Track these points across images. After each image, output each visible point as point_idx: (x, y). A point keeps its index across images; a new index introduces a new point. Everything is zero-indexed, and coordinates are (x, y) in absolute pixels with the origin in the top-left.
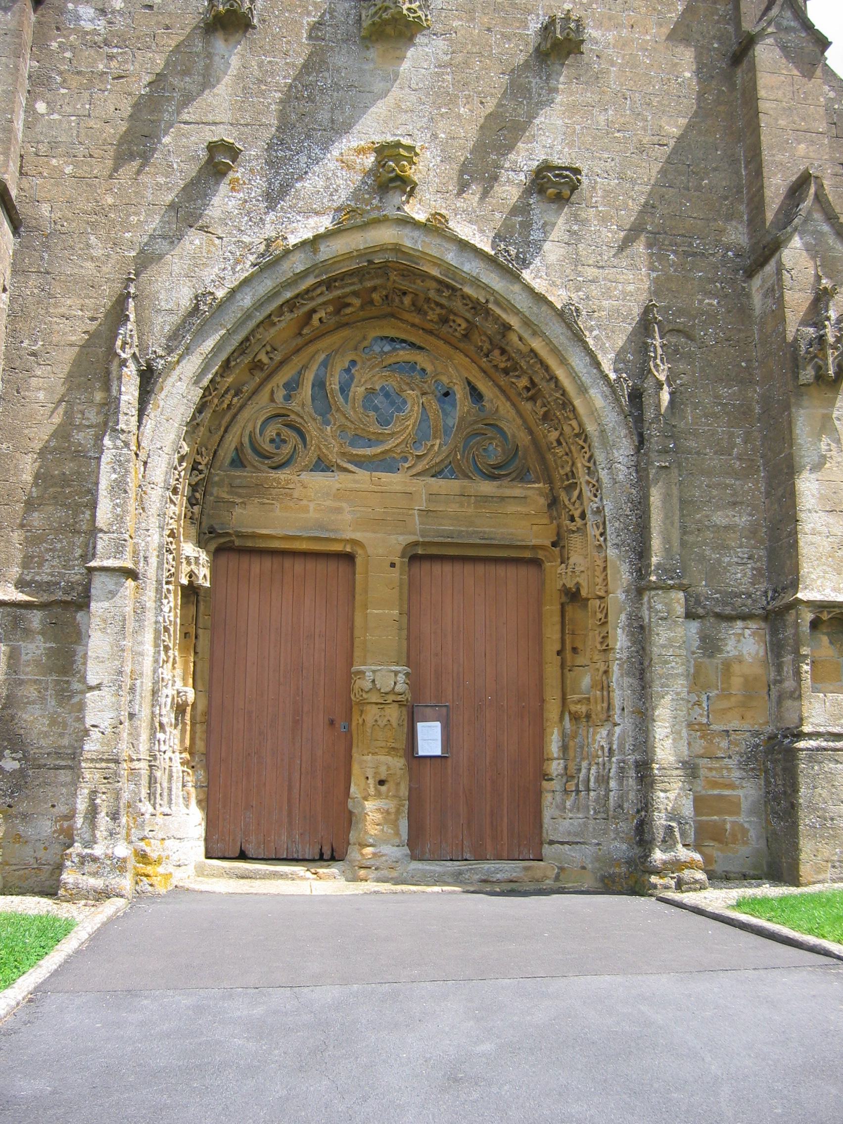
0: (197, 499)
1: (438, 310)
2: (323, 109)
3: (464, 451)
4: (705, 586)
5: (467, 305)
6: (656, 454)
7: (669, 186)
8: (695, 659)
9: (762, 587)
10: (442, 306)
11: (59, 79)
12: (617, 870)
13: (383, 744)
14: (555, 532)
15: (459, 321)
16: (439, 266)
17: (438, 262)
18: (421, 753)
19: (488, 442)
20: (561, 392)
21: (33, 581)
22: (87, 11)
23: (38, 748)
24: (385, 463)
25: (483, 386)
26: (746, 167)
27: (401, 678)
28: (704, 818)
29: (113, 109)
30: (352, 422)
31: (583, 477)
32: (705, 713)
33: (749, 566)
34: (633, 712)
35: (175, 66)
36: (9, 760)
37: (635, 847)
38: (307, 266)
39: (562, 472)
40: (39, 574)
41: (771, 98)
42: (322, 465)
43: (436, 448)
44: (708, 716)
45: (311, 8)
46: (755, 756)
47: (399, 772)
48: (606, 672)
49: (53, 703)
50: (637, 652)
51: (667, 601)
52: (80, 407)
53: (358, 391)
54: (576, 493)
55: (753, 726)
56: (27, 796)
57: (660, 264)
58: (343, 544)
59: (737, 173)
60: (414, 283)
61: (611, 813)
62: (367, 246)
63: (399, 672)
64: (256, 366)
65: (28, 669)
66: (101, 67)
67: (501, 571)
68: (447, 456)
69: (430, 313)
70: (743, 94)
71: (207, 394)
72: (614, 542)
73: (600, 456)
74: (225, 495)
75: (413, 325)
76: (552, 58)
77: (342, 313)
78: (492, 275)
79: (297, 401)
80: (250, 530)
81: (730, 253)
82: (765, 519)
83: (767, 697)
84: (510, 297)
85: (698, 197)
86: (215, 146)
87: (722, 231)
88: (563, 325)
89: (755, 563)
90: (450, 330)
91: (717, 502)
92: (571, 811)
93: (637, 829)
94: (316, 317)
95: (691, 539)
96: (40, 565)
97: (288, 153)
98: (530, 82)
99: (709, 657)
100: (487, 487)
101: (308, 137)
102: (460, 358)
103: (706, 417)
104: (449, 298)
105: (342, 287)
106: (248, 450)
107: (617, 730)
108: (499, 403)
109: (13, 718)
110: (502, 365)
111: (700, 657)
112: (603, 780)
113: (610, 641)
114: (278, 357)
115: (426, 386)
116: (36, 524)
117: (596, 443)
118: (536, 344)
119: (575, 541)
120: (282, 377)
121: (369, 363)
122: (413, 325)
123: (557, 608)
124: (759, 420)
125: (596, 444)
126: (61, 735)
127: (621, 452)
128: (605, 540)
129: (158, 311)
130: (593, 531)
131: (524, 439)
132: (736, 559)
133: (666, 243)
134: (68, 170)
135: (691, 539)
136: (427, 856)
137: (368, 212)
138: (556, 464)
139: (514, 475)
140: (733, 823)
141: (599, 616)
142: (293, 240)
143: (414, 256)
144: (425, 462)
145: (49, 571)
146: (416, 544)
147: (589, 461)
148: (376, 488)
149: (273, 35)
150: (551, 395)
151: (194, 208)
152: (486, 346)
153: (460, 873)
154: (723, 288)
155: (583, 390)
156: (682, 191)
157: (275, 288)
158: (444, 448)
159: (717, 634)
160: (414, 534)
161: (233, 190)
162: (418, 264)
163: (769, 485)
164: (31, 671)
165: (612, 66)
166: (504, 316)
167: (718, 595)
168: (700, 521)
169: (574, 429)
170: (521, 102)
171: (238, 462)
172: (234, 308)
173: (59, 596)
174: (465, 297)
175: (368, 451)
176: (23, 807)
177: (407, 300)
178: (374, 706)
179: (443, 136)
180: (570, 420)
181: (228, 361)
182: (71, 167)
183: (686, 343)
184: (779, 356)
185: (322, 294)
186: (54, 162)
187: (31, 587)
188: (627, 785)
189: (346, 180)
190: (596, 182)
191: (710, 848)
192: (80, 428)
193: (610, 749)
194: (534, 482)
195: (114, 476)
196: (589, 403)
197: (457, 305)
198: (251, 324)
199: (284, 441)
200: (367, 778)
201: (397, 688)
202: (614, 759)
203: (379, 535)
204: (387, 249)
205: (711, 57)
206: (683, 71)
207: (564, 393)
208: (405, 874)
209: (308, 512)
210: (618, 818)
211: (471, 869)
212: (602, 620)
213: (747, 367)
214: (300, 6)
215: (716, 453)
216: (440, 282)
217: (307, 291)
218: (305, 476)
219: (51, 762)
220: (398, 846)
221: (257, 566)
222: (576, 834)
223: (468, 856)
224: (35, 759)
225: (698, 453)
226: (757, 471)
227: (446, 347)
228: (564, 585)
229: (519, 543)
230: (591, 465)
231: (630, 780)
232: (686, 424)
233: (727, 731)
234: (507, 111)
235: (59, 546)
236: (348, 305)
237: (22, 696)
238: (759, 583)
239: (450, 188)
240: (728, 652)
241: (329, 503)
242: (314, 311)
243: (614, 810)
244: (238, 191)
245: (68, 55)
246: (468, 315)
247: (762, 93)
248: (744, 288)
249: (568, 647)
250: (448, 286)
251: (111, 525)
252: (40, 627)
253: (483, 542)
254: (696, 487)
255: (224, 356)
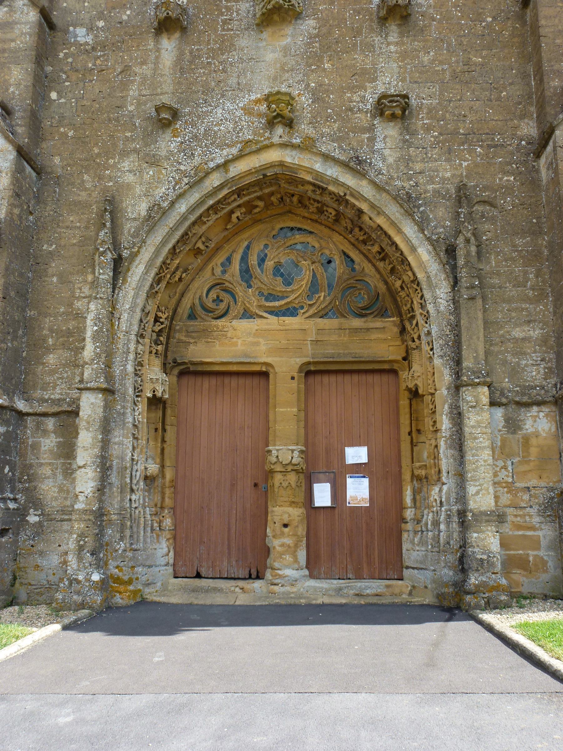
0: (161, 341)
1: (316, 205)
2: (233, 76)
3: (341, 300)
4: (508, 382)
5: (333, 198)
6: (465, 290)
7: (477, 100)
8: (501, 436)
9: (553, 381)
10: (318, 202)
11: (64, 76)
12: (446, 590)
13: (286, 499)
14: (405, 350)
15: (330, 210)
16: (311, 173)
17: (310, 171)
18: (317, 504)
19: (357, 292)
20: (400, 252)
21: (50, 399)
22: (81, 32)
23: (51, 508)
24: (290, 311)
25: (354, 254)
26: (534, 79)
27: (296, 454)
28: (512, 552)
29: (98, 91)
30: (265, 285)
31: (418, 311)
32: (510, 474)
33: (542, 366)
34: (455, 475)
35: (137, 59)
36: (32, 516)
37: (460, 573)
38: (221, 182)
39: (405, 308)
40: (53, 394)
41: (550, 24)
42: (247, 314)
43: (322, 298)
44: (513, 477)
45: (224, 10)
46: (551, 506)
47: (297, 519)
48: (436, 446)
49: (61, 478)
50: (457, 431)
51: (475, 394)
52: (79, 285)
53: (270, 264)
54: (414, 322)
55: (548, 483)
56: (43, 540)
57: (470, 156)
58: (260, 366)
59: (529, 84)
60: (297, 187)
61: (441, 548)
62: (261, 164)
63: (294, 450)
64: (198, 252)
65: (46, 456)
66: (90, 65)
67: (370, 378)
68: (330, 303)
69: (311, 207)
70: (531, 28)
71: (161, 271)
72: (439, 354)
73: (428, 295)
74: (183, 338)
75: (304, 217)
76: (389, 21)
77: (253, 213)
78: (347, 176)
79: (229, 274)
80: (199, 360)
81: (523, 143)
82: (554, 331)
83: (559, 462)
84: (360, 190)
85: (499, 105)
86: (159, 108)
87: (516, 127)
88: (398, 205)
89: (547, 364)
90: (326, 218)
91: (515, 321)
92: (418, 545)
93: (460, 560)
94: (234, 216)
95: (496, 349)
96: (54, 388)
97: (210, 108)
98: (374, 41)
99: (512, 433)
100: (357, 323)
101: (223, 96)
102: (337, 238)
103: (506, 260)
104: (321, 194)
105: (249, 194)
106: (199, 308)
107: (445, 488)
108: (364, 265)
109: (35, 488)
110: (361, 238)
111: (505, 434)
112: (436, 523)
113: (438, 425)
114: (212, 245)
115: (314, 257)
116: (51, 362)
117: (424, 286)
118: (380, 221)
119: (415, 355)
120: (220, 258)
121: (276, 245)
122: (304, 217)
123: (407, 402)
124: (547, 260)
125: (425, 287)
126: (66, 499)
127: (442, 290)
128: (434, 354)
129: (128, 219)
130: (426, 348)
131: (382, 288)
132: (531, 362)
133: (475, 140)
134: (71, 134)
135: (496, 349)
136: (323, 575)
137: (262, 142)
138: (402, 303)
139: (375, 313)
140: (535, 556)
141: (431, 406)
142: (212, 165)
143: (294, 168)
144: (314, 308)
145: (59, 392)
146: (309, 363)
147: (421, 299)
148: (282, 328)
149: (199, 31)
150: (394, 256)
151: (149, 151)
152: (350, 226)
153: (340, 589)
154: (518, 168)
155: (413, 249)
156: (486, 102)
157: (201, 198)
158: (328, 298)
159: (518, 417)
160: (307, 357)
161: (174, 136)
162: (297, 174)
163: (555, 306)
164: (47, 457)
165: (433, 21)
166: (357, 203)
167: (518, 389)
168: (503, 336)
169: (410, 278)
170: (368, 55)
171: (192, 316)
172: (174, 214)
173: (65, 408)
174: (331, 193)
175: (277, 304)
176: (41, 546)
177: (295, 199)
178: (279, 473)
179: (313, 85)
180: (407, 271)
181: (174, 248)
182: (72, 131)
183: (490, 210)
184: (557, 211)
185: (235, 200)
186: (62, 130)
187: (48, 402)
188: (452, 527)
189: (248, 122)
190: (422, 104)
191: (517, 575)
192: (78, 298)
193: (441, 502)
194: (390, 317)
195: (95, 328)
196: (418, 258)
197: (327, 199)
198: (187, 224)
199: (222, 301)
200: (275, 523)
201: (293, 461)
202: (443, 509)
203: (283, 359)
204: (275, 165)
205: (507, 4)
206: (486, 17)
207: (402, 253)
208: (302, 590)
209: (237, 345)
210: (446, 552)
211: (349, 586)
212: (433, 410)
213: (538, 222)
214: (216, 10)
215: (514, 286)
216: (314, 185)
217: (225, 198)
218: (235, 323)
219: (59, 517)
220: (297, 570)
221: (207, 383)
222: (421, 563)
223: (350, 576)
224: (48, 515)
225: (500, 287)
226: (547, 297)
227: (326, 231)
228: (407, 386)
229: (379, 359)
230: (423, 301)
231: (454, 524)
232: (491, 267)
233: (528, 488)
234: (358, 62)
235: (65, 375)
236: (257, 206)
237: (41, 474)
238: (550, 378)
239: (319, 120)
240: (527, 430)
241: (251, 339)
242: (232, 212)
243: (444, 546)
244: (177, 137)
245: (70, 60)
246: (335, 206)
247: (543, 22)
248: (534, 166)
249: (414, 429)
250: (319, 187)
251: (93, 360)
252: (53, 428)
253: (353, 360)
254: (499, 311)
255: (170, 246)
